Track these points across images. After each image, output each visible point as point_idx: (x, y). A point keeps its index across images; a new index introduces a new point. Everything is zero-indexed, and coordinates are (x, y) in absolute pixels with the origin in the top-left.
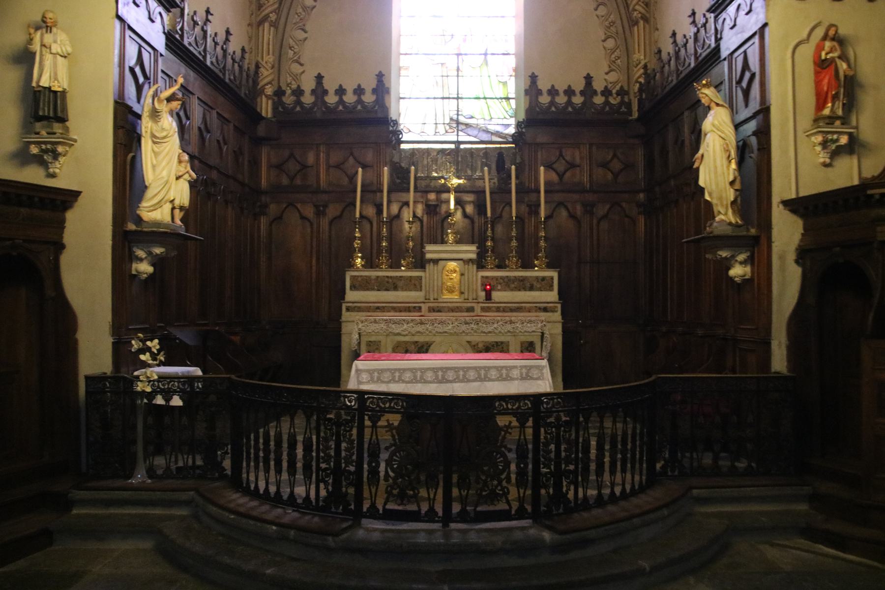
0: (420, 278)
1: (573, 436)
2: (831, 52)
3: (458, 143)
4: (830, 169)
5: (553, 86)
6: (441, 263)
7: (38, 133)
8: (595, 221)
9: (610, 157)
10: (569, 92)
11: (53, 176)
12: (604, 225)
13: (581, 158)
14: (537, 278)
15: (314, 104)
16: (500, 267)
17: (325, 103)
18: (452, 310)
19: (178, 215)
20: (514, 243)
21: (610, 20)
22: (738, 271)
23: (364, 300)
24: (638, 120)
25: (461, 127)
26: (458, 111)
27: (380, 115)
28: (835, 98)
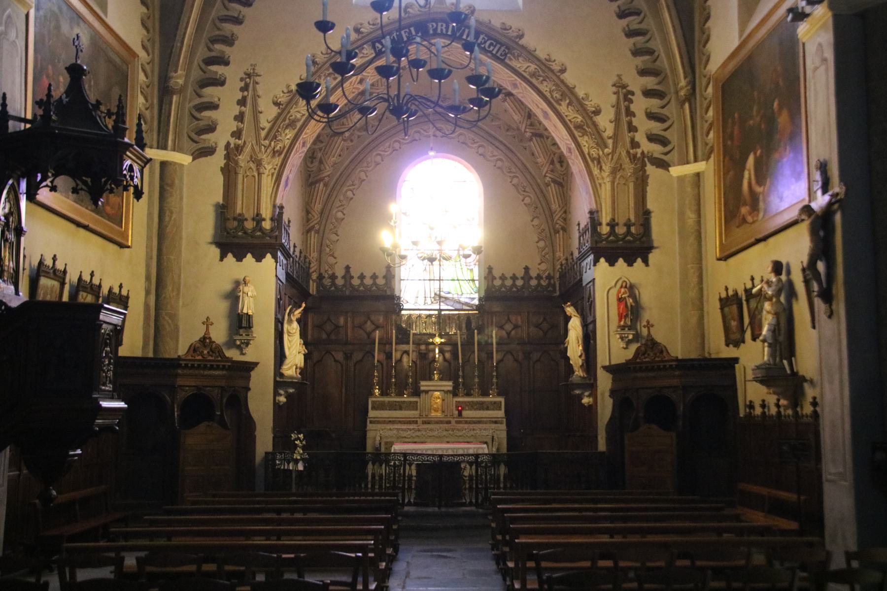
0: (417, 402)
1: (493, 473)
2: (624, 294)
3: (440, 310)
4: (626, 350)
7: (242, 335)
9: (541, 320)
10: (514, 278)
11: (244, 354)
14: (491, 402)
15: (344, 285)
16: (468, 394)
17: (351, 284)
18: (437, 423)
19: (298, 371)
20: (477, 380)
21: (541, 228)
22: (586, 401)
24: (559, 297)
25: (442, 299)
26: (440, 289)
27: (389, 293)
28: (626, 316)
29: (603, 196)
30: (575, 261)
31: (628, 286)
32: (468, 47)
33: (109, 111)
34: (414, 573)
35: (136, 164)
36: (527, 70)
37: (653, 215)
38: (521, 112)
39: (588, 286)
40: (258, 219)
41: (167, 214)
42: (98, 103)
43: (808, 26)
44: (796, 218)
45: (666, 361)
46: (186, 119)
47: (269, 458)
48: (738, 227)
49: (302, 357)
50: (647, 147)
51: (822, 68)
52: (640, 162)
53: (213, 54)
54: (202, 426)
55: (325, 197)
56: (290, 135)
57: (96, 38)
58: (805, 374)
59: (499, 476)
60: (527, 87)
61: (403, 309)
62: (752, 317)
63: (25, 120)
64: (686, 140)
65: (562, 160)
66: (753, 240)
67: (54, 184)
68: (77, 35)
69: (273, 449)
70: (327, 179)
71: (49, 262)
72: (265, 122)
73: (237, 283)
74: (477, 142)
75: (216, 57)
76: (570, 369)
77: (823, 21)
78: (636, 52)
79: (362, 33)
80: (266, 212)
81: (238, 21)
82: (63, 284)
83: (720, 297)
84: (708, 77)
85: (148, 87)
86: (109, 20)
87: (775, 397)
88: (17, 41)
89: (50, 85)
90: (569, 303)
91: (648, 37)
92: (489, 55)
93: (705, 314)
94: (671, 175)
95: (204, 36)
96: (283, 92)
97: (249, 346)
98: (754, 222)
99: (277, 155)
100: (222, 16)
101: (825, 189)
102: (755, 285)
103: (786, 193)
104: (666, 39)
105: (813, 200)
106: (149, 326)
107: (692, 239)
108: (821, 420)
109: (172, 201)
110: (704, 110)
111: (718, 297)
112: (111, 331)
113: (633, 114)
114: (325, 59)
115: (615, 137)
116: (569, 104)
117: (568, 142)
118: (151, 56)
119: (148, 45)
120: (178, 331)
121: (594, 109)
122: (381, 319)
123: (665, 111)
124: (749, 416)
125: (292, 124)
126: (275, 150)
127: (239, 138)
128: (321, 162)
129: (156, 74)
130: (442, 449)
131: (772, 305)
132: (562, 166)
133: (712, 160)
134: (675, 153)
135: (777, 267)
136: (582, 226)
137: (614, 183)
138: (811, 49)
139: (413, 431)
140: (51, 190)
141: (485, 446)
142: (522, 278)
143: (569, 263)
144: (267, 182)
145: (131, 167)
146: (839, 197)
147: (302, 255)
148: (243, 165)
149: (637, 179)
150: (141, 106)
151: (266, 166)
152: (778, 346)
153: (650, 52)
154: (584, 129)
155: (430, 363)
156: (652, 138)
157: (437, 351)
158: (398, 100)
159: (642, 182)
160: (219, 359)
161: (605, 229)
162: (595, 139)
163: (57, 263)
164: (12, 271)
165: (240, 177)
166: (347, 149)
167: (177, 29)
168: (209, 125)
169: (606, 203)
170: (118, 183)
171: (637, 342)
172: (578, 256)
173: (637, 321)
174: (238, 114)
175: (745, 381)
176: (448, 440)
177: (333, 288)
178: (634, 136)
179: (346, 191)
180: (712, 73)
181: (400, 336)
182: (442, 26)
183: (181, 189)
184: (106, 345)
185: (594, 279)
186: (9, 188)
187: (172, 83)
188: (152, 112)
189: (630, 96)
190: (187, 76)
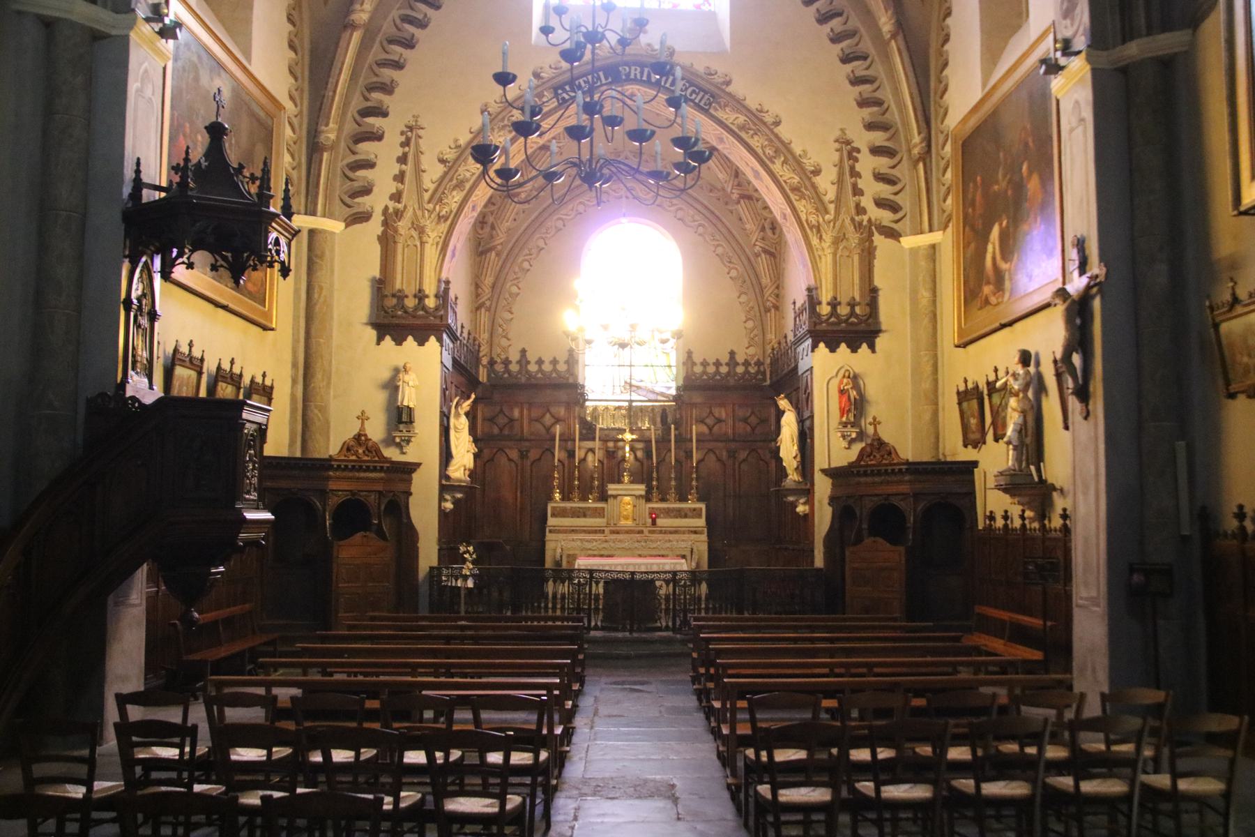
0: (603, 509)
3: (631, 401)
4: (849, 450)
5: (705, 359)
6: (619, 498)
8: (737, 464)
9: (749, 414)
11: (404, 453)
12: (744, 467)
13: (727, 414)
14: (690, 509)
15: (520, 372)
16: (663, 500)
17: (527, 372)
18: (627, 532)
19: (467, 473)
20: (673, 483)
22: (801, 509)
23: (561, 524)
24: (770, 386)
25: (633, 389)
27: (571, 381)
28: (849, 411)
29: (823, 270)
30: (789, 345)
31: (851, 376)
32: (674, 102)
33: (252, 175)
34: (603, 710)
35: (282, 237)
36: (735, 122)
37: (880, 293)
38: (728, 170)
39: (805, 375)
40: (421, 296)
41: (316, 291)
42: (241, 167)
43: (1063, 81)
44: (1048, 300)
45: (895, 464)
46: (338, 181)
47: (434, 573)
48: (979, 309)
49: (472, 457)
50: (875, 213)
51: (1080, 130)
52: (867, 231)
53: (369, 104)
54: (358, 537)
55: (498, 268)
56: (458, 197)
57: (238, 89)
58: (1055, 483)
59: (700, 598)
60: (734, 141)
61: (588, 400)
62: (995, 414)
63: (159, 188)
64: (920, 206)
65: (774, 226)
66: (997, 325)
67: (191, 261)
68: (219, 90)
69: (439, 564)
70: (499, 247)
71: (184, 349)
72: (428, 183)
73: (397, 371)
74: (676, 205)
75: (374, 107)
76: (782, 472)
77: (1081, 75)
78: (863, 103)
79: (542, 78)
80: (430, 288)
81: (398, 66)
82: (200, 373)
83: (958, 390)
84: (945, 133)
85: (295, 143)
86: (252, 69)
87: (1020, 508)
88: (153, 99)
89: (188, 148)
90: (782, 396)
91: (876, 85)
92: (692, 104)
93: (940, 409)
94: (902, 247)
95: (360, 83)
96: (450, 147)
97: (411, 444)
98: (998, 304)
99: (442, 220)
100: (381, 60)
101: (1083, 269)
102: (999, 377)
103: (1036, 272)
104: (897, 88)
105: (1069, 282)
106: (296, 420)
107: (926, 321)
108: (1073, 537)
109: (322, 276)
110: (941, 171)
111: (955, 390)
112: (255, 431)
113: (858, 175)
114: (500, 109)
115: (838, 201)
116: (785, 162)
117: (784, 207)
118: (299, 108)
119: (296, 94)
120: (329, 427)
121: (813, 168)
122: (562, 412)
123: (895, 172)
124: (989, 529)
125: (460, 185)
126: (441, 215)
127: (399, 202)
128: (493, 227)
129: (305, 126)
130: (634, 565)
131: (1018, 401)
132: (774, 234)
133: (949, 230)
134: (907, 221)
135: (1025, 358)
136: (798, 305)
137: (836, 255)
138: (1066, 107)
139: (599, 542)
140: (187, 268)
141: (684, 561)
142: (727, 364)
143: (782, 347)
144: (431, 253)
145: (277, 240)
146: (1098, 280)
147: (471, 337)
148: (403, 233)
149: (863, 250)
150: (287, 165)
151: (430, 233)
152: (1025, 449)
153: (879, 103)
154: (800, 191)
155: (619, 463)
156: (880, 203)
157: (627, 448)
158: (590, 166)
159: (868, 254)
160: (377, 459)
161: (825, 310)
162: (815, 203)
163: (193, 349)
164: (145, 362)
165: (400, 247)
166: (524, 212)
167: (329, 76)
168: (364, 186)
169: (826, 280)
170: (262, 260)
171: (862, 440)
172: (793, 340)
173: (861, 417)
174: (398, 173)
175: (985, 488)
176: (640, 553)
177: (506, 375)
178: (860, 201)
179: (522, 262)
180: (951, 129)
181: (584, 432)
182: (636, 70)
183: (332, 260)
184: (250, 449)
185: (812, 367)
186: (143, 267)
187: (322, 138)
188: (300, 172)
189: (855, 154)
190: (340, 130)
